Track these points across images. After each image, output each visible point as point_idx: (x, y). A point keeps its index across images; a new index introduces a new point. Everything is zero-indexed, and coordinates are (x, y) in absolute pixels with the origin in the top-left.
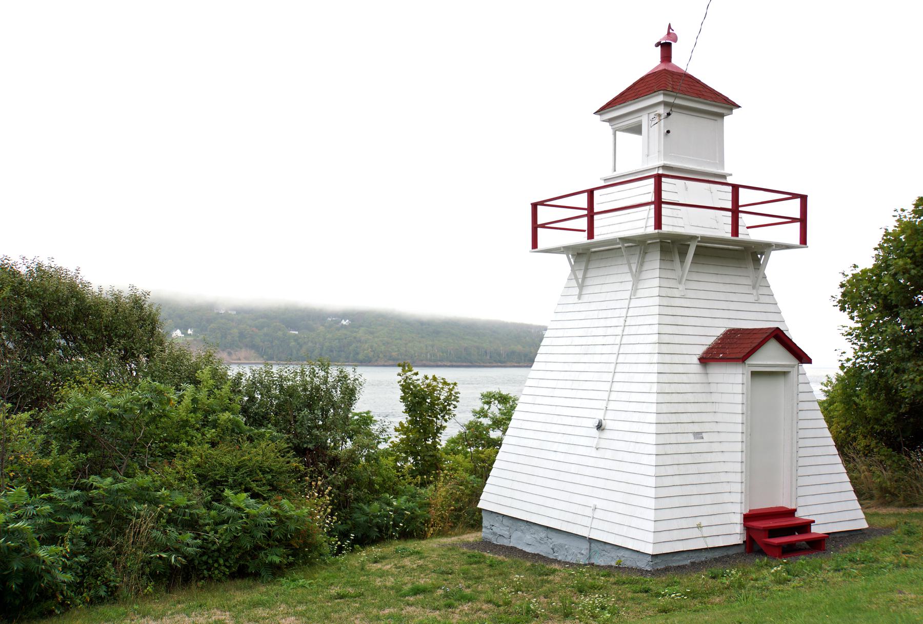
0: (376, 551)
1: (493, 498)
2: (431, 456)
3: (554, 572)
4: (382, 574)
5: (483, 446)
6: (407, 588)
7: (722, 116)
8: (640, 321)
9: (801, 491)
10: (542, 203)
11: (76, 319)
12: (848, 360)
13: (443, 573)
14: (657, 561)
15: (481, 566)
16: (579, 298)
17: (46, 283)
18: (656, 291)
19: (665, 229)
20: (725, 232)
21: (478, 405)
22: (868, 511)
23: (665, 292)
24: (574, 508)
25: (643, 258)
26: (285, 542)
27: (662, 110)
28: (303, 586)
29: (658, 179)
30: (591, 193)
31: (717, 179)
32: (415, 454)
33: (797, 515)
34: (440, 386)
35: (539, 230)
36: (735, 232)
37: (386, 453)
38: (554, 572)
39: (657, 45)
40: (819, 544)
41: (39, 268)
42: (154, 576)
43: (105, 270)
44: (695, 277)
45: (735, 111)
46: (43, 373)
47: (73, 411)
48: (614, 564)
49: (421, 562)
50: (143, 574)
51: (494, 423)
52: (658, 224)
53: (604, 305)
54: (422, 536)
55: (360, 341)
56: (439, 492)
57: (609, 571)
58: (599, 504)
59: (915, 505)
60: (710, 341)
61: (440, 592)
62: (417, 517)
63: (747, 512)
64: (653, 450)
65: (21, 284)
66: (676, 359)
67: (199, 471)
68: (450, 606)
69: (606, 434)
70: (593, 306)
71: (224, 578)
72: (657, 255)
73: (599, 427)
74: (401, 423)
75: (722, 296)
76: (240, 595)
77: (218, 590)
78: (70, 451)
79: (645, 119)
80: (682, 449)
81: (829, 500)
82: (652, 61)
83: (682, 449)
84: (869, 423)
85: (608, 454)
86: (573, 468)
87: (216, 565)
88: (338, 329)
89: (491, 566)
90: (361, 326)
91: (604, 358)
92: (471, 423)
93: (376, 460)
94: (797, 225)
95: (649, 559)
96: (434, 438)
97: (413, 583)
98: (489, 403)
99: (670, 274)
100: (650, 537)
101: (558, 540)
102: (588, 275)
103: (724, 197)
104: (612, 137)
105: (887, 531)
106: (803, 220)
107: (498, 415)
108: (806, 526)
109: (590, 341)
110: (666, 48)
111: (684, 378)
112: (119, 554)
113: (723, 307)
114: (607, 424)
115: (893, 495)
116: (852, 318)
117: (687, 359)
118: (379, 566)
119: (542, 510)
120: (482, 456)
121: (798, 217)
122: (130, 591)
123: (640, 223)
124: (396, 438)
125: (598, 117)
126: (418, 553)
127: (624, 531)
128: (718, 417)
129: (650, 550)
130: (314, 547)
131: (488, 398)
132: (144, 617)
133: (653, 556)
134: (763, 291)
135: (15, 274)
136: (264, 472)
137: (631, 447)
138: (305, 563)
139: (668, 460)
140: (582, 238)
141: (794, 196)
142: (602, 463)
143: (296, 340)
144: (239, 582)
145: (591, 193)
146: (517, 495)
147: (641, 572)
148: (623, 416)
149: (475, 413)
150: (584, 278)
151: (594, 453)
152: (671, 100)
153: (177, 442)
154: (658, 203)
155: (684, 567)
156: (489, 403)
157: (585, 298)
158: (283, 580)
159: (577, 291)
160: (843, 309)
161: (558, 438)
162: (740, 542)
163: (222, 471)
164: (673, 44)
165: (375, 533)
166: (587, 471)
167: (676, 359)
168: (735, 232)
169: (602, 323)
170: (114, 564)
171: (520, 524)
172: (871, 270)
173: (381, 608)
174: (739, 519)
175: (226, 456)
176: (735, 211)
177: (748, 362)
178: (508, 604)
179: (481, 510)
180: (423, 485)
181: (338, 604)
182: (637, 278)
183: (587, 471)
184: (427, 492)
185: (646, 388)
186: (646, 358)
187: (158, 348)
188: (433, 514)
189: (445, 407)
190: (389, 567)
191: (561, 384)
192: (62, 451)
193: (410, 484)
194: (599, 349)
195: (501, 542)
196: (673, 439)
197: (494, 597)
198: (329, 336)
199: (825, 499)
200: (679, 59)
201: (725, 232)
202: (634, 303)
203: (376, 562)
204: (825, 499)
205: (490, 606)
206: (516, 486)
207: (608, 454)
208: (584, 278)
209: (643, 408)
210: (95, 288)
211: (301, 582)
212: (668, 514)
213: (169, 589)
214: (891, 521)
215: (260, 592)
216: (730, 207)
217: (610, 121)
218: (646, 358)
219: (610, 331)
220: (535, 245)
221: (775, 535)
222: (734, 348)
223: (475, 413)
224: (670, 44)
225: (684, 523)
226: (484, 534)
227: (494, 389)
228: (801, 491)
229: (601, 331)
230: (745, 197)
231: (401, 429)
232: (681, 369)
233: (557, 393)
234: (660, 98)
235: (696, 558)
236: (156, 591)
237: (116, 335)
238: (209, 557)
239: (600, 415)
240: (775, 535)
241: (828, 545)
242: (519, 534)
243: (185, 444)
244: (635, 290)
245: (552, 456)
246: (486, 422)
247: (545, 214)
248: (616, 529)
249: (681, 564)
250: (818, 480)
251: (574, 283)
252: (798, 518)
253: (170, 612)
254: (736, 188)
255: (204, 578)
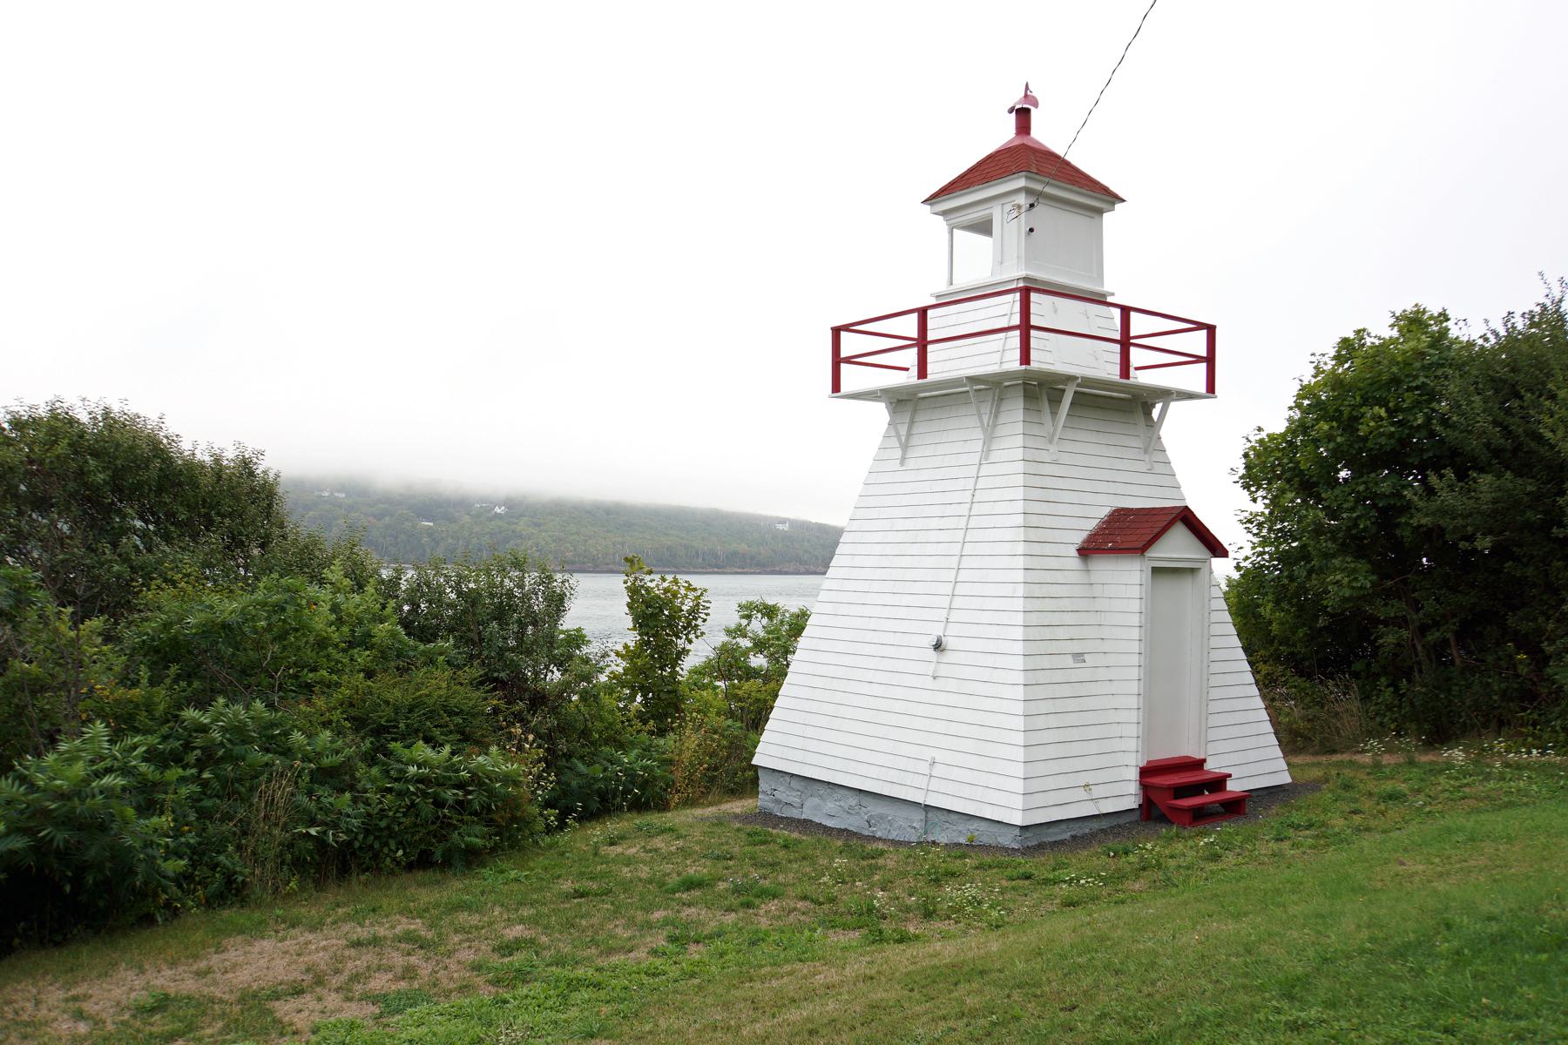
0: (613, 826)
1: (770, 751)
2: (669, 692)
3: (882, 853)
4: (628, 861)
5: (740, 679)
6: (674, 880)
7: (1100, 212)
8: (996, 494)
9: (1212, 734)
10: (847, 328)
11: (160, 490)
12: (1247, 558)
13: (718, 858)
14: (1028, 834)
15: (771, 846)
16: (902, 463)
17: (118, 436)
18: (1019, 454)
19: (1034, 365)
20: (1112, 372)
21: (734, 620)
22: (1299, 760)
23: (1031, 455)
24: (902, 763)
25: (998, 407)
26: (484, 815)
27: (1022, 200)
28: (517, 880)
29: (1025, 293)
30: (923, 313)
31: (1100, 300)
32: (644, 690)
33: (1207, 766)
34: (683, 591)
35: (843, 366)
36: (1125, 372)
37: (609, 689)
38: (882, 853)
39: (1011, 111)
40: (1236, 806)
41: (107, 413)
42: (298, 865)
43: (201, 422)
44: (1070, 434)
45: (1118, 206)
46: (116, 568)
47: (166, 626)
48: (962, 840)
49: (680, 843)
50: (283, 863)
51: (756, 645)
52: (1025, 358)
53: (940, 474)
54: (663, 807)
55: (521, 537)
56: (685, 744)
57: (959, 850)
58: (939, 756)
59: (1334, 752)
60: (1092, 525)
61: (722, 886)
62: (655, 779)
63: (1143, 764)
64: (1020, 678)
65: (81, 437)
66: (1048, 549)
67: (353, 712)
68: (748, 905)
69: (948, 657)
70: (924, 475)
71: (397, 870)
72: (1019, 404)
73: (938, 646)
74: (626, 647)
75: (1105, 463)
76: (427, 893)
77: (390, 887)
78: (168, 681)
79: (997, 213)
80: (1059, 676)
81: (1243, 743)
82: (1003, 133)
83: (1059, 676)
84: (1272, 642)
85: (952, 685)
86: (898, 706)
87: (386, 850)
88: (491, 520)
89: (786, 847)
90: (522, 515)
91: (941, 549)
92: (724, 645)
93: (596, 697)
94: (1203, 366)
95: (1017, 832)
96: (673, 667)
97: (679, 874)
98: (749, 617)
99: (1036, 430)
100: (1018, 802)
101: (876, 809)
102: (915, 431)
103: (1111, 323)
104: (946, 236)
105: (1314, 786)
106: (1210, 360)
107: (762, 634)
108: (1219, 782)
109: (920, 524)
110: (1023, 116)
111: (1059, 577)
112: (245, 833)
113: (1105, 480)
114: (949, 642)
115: (1307, 739)
116: (1254, 500)
117: (1061, 550)
118: (619, 849)
119: (852, 767)
120: (740, 693)
121: (1204, 354)
122: (265, 889)
123: (1002, 356)
124: (619, 666)
125: (927, 208)
126: (671, 830)
127: (978, 793)
128: (1105, 632)
129: (1018, 819)
130: (526, 823)
131: (748, 611)
132: (293, 926)
133: (1022, 828)
134: (1158, 457)
135: (72, 422)
136: (451, 713)
137: (986, 674)
138: (512, 847)
139: (1040, 692)
140: (910, 378)
141: (1200, 326)
142: (942, 698)
143: (430, 535)
144: (420, 875)
145: (923, 313)
146: (813, 745)
147: (1006, 850)
148: (974, 631)
149: (729, 632)
150: (909, 435)
151: (929, 683)
152: (1038, 187)
153: (314, 670)
154: (1025, 327)
155: (1062, 843)
156: (749, 617)
157: (911, 464)
158: (486, 872)
159: (898, 453)
160: (1246, 487)
161: (873, 663)
162: (1135, 806)
163: (389, 711)
164: (1033, 110)
165: (595, 805)
166: (920, 710)
167: (1048, 549)
168: (1125, 372)
169: (939, 498)
170: (239, 848)
171: (817, 786)
172: (1283, 435)
173: (648, 909)
174: (1134, 774)
175: (392, 691)
176: (1126, 342)
177: (1151, 553)
178: (832, 900)
179: (756, 767)
180: (662, 733)
181: (580, 905)
182: (990, 438)
183: (920, 710)
184: (668, 742)
185: (1007, 590)
186: (1006, 548)
187: (276, 531)
188: (678, 775)
189: (689, 624)
190: (633, 850)
191: (876, 586)
192: (152, 683)
193: (639, 732)
194: (933, 536)
195: (788, 812)
196: (1046, 662)
197: (809, 889)
198: (477, 529)
199: (1240, 744)
200: (1044, 132)
201: (1112, 372)
202: (985, 470)
203: (612, 844)
204: (1240, 744)
205: (808, 903)
206: (810, 732)
207: (952, 685)
208: (909, 435)
209: (1004, 618)
210: (186, 446)
211: (513, 874)
212: (1040, 769)
213: (320, 885)
214: (1317, 773)
215: (455, 888)
216: (1118, 337)
217: (944, 213)
218: (1006, 548)
219: (949, 510)
220: (836, 387)
221: (1179, 795)
222: (1125, 534)
223: (729, 632)
224: (1028, 111)
225: (1062, 781)
226: (763, 801)
227: (755, 599)
228: (1212, 734)
229: (936, 511)
230: (1139, 324)
231: (629, 655)
232: (1053, 563)
233: (869, 599)
234: (1020, 182)
235: (1078, 830)
236: (302, 888)
237: (218, 514)
238: (376, 838)
239: (937, 630)
240: (1179, 795)
241: (1249, 806)
242: (816, 800)
243: (324, 673)
244: (986, 452)
245: (865, 689)
246: (745, 643)
247: (851, 344)
248: (967, 791)
249: (1059, 838)
250: (1231, 718)
251: (894, 442)
252: (1208, 772)
253: (329, 920)
254: (1126, 311)
255: (367, 869)
